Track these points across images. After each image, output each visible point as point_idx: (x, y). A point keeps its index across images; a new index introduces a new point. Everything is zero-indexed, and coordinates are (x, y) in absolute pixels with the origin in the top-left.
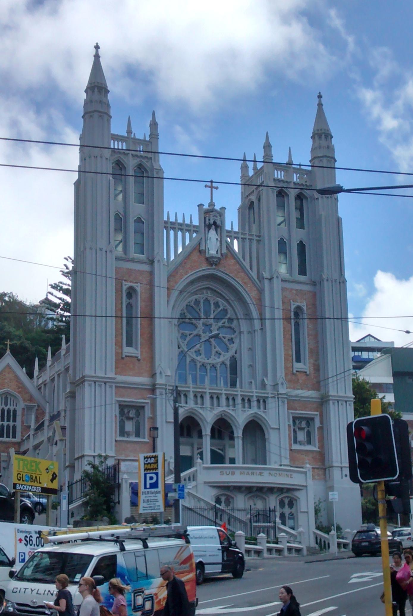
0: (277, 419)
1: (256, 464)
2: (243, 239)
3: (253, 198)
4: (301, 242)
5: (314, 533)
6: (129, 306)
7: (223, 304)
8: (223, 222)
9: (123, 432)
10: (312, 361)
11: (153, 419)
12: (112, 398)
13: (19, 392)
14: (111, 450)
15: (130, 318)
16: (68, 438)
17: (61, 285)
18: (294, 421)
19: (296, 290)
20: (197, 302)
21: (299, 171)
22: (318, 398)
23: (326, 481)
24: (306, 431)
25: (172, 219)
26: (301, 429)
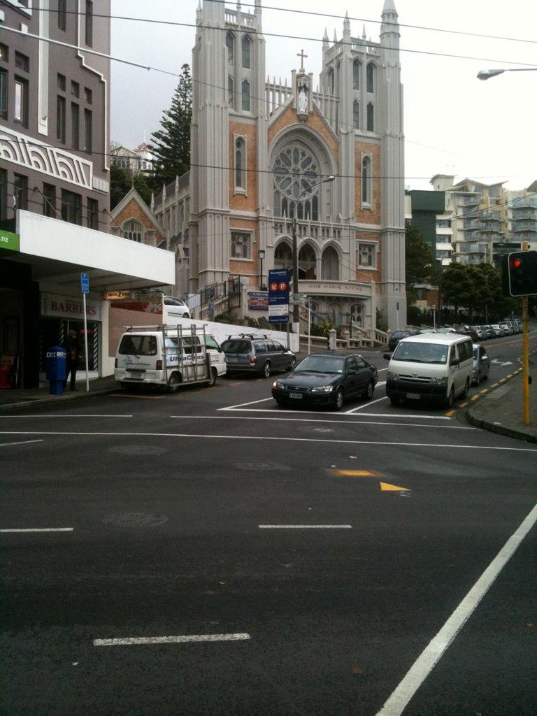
0: (348, 246)
1: (330, 279)
2: (326, 100)
3: (333, 65)
4: (370, 104)
5: (375, 331)
6: (239, 153)
7: (308, 154)
8: (310, 85)
9: (234, 254)
10: (375, 201)
11: (257, 244)
12: (227, 227)
13: (143, 221)
14: (227, 266)
15: (365, 177)
16: (190, 257)
17: (160, 133)
18: (360, 248)
19: (366, 143)
20: (289, 152)
21: (370, 45)
22: (255, 218)
23: (381, 293)
24: (368, 255)
25: (271, 82)
26: (365, 254)
